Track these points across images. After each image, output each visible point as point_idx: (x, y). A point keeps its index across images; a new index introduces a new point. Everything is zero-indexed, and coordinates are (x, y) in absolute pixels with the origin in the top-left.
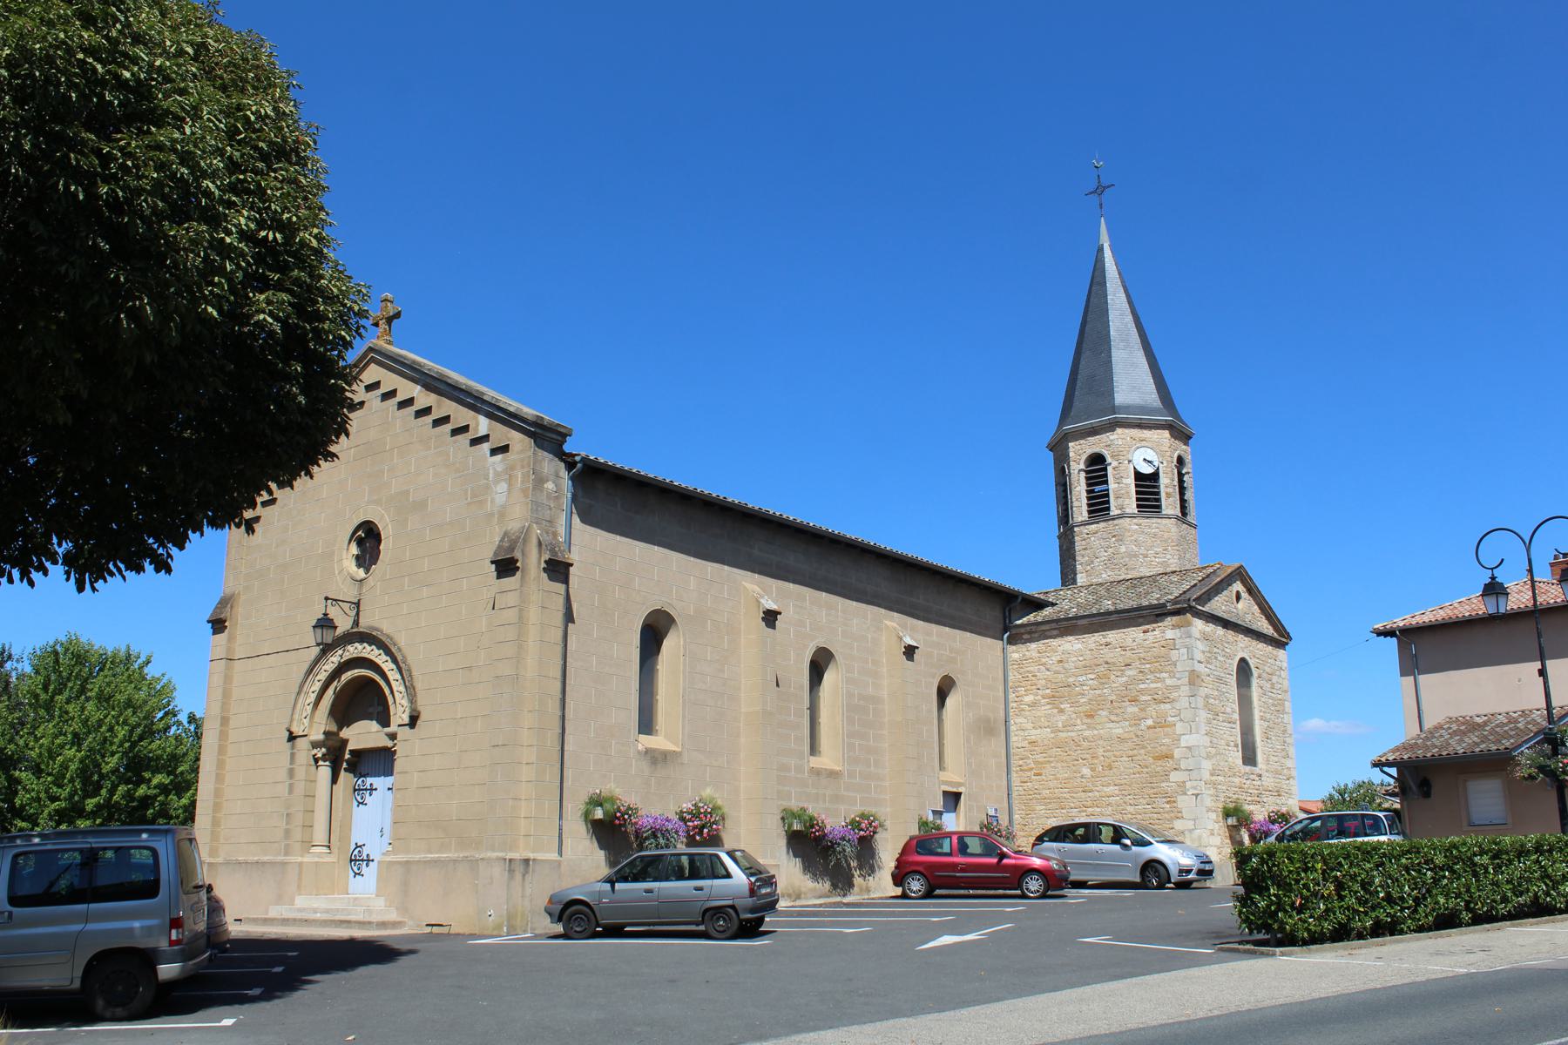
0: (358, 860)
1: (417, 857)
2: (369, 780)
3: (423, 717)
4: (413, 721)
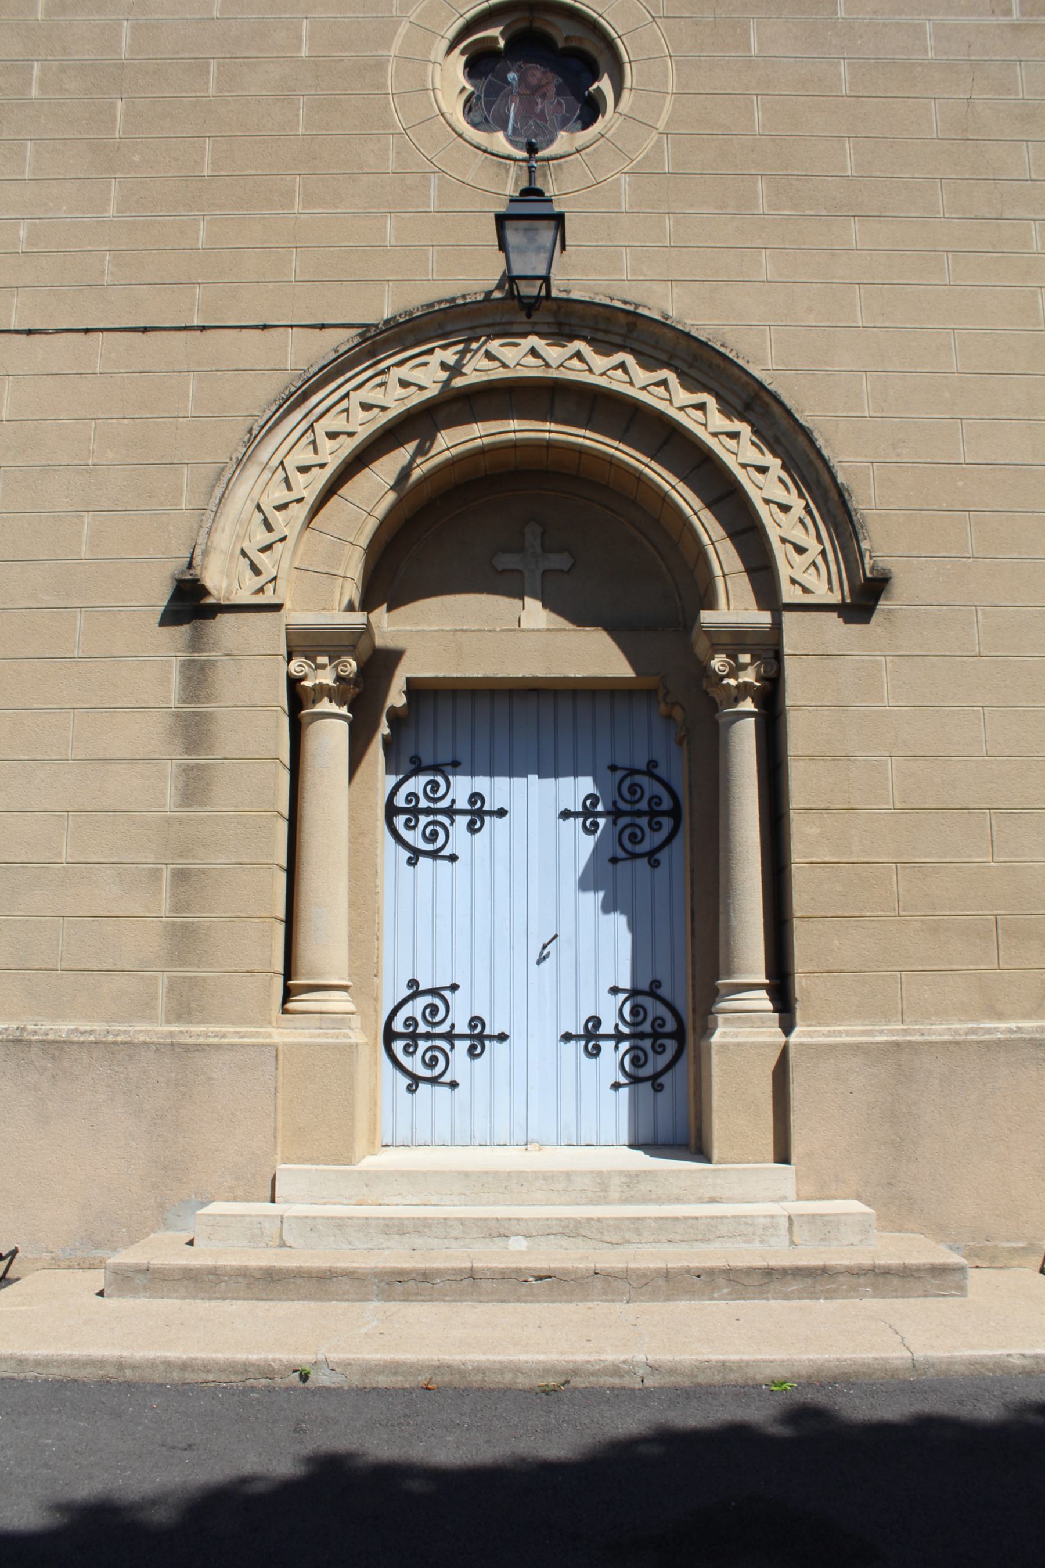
0: (424, 1037)
1: (940, 1030)
2: (460, 788)
3: (901, 589)
4: (864, 597)
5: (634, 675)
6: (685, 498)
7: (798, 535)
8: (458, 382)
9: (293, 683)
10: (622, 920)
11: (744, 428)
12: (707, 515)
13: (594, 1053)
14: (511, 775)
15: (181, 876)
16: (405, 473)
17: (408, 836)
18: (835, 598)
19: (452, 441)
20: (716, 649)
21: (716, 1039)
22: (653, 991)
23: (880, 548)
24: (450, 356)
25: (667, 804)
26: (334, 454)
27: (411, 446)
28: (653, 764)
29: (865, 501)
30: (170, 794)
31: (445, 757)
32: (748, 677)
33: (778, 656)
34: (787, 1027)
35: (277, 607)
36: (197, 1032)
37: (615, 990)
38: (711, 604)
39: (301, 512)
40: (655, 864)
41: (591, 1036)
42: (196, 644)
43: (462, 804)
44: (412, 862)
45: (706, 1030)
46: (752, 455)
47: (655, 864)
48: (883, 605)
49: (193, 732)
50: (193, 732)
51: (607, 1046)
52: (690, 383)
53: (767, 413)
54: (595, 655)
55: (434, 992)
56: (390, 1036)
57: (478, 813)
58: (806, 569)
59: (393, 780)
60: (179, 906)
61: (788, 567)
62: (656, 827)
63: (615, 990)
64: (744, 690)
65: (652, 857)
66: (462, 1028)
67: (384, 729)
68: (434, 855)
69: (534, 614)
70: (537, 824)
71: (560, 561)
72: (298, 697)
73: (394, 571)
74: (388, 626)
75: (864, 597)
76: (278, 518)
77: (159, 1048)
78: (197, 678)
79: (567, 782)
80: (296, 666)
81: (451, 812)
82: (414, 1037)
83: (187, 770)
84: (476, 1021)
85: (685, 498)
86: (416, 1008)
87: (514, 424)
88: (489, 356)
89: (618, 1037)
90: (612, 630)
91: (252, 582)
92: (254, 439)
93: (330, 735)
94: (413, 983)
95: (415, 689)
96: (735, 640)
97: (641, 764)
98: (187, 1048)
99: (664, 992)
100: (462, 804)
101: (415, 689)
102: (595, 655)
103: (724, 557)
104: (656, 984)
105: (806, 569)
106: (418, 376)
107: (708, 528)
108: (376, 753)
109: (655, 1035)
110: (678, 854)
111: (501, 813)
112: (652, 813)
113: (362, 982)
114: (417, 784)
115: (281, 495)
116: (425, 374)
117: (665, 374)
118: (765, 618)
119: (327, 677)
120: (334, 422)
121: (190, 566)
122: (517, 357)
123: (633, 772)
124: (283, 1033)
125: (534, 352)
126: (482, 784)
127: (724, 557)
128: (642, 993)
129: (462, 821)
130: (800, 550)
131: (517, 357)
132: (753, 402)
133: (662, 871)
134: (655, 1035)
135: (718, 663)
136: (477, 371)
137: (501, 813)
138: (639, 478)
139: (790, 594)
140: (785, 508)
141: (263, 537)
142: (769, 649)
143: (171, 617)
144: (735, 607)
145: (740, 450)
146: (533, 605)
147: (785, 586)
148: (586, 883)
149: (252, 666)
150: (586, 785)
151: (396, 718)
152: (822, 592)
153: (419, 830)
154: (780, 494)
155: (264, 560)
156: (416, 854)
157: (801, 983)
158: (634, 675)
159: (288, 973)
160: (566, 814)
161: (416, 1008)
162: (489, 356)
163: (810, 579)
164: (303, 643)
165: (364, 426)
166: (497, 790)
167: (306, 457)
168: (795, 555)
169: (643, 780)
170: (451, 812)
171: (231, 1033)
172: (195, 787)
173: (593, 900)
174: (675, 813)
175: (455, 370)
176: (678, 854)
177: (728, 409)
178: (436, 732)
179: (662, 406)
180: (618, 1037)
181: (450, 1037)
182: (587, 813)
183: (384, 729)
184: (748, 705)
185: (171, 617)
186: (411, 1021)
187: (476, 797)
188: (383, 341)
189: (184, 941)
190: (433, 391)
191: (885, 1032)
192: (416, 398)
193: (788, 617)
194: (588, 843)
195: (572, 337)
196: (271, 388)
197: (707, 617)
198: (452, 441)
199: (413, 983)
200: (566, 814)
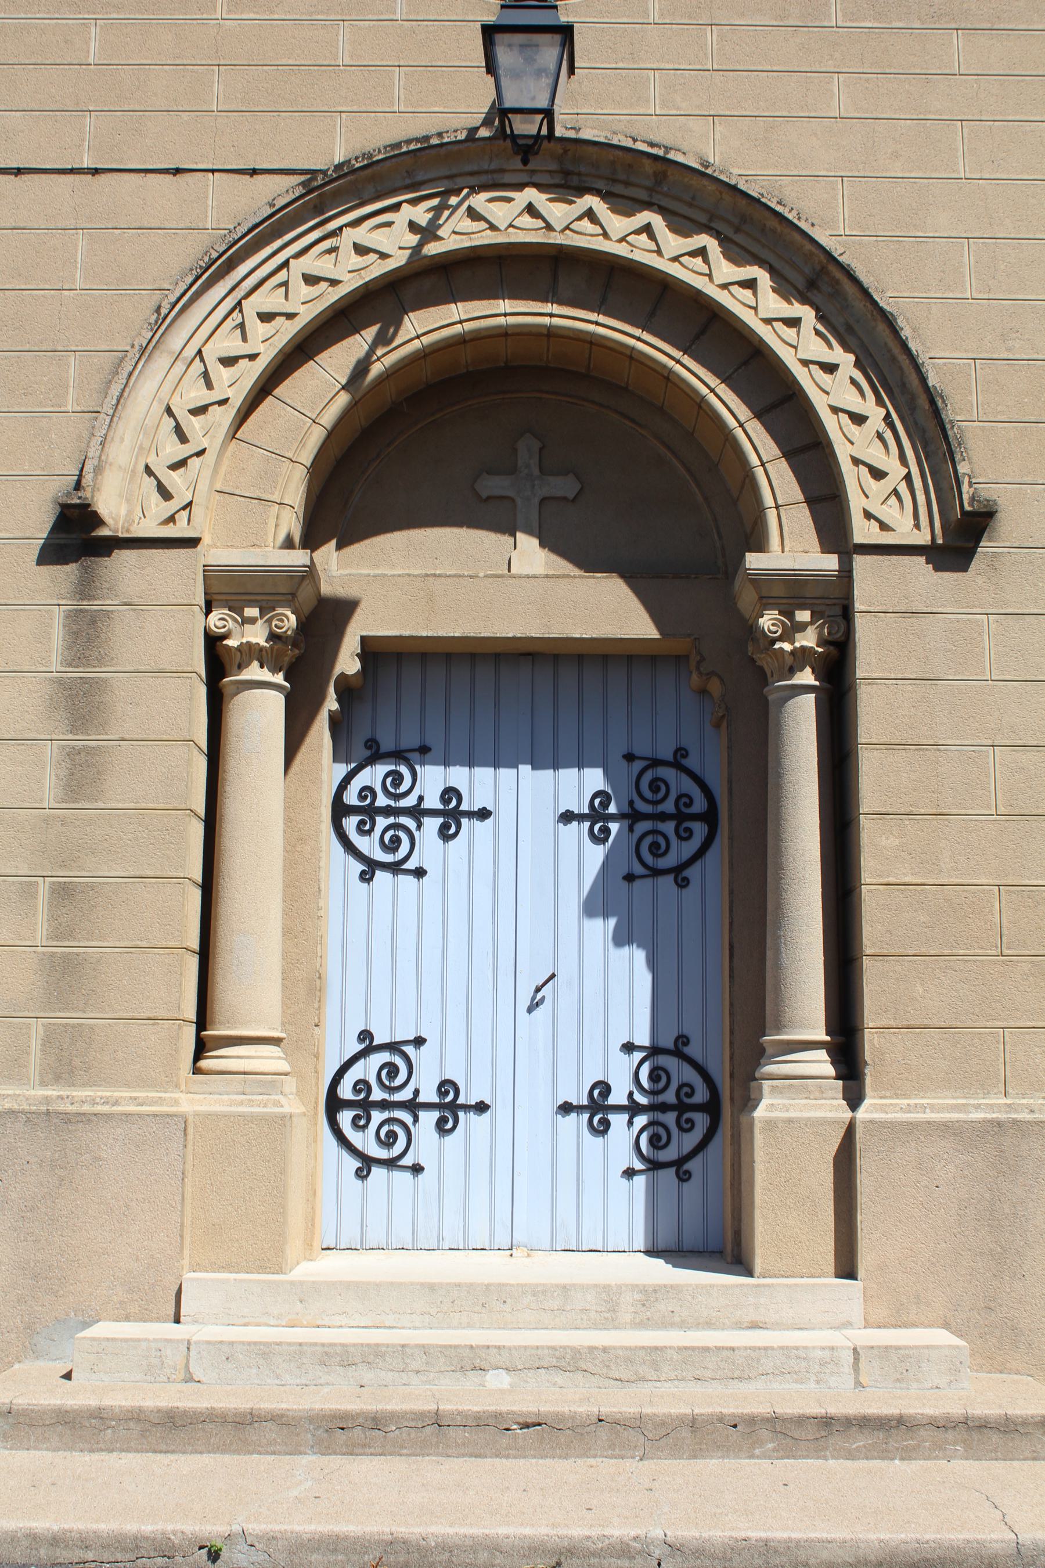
2: (431, 781)
5: (658, 637)
6: (729, 406)
7: (875, 455)
8: (432, 249)
9: (213, 642)
10: (640, 956)
11: (807, 314)
12: (756, 428)
13: (602, 1129)
14: (496, 765)
15: (63, 893)
16: (362, 368)
17: (362, 843)
18: (923, 538)
19: (425, 326)
20: (765, 603)
21: (760, 1113)
22: (679, 1049)
23: (986, 469)
24: (421, 214)
25: (699, 805)
26: (269, 342)
27: (370, 333)
28: (681, 752)
29: (962, 410)
30: (48, 787)
31: (410, 740)
32: (808, 639)
33: (846, 613)
34: (854, 1100)
35: (192, 542)
36: (80, 1097)
37: (629, 1048)
38: (760, 546)
39: (223, 417)
40: (683, 883)
41: (597, 1107)
42: (85, 589)
43: (433, 802)
44: (366, 877)
45: (748, 1101)
46: (816, 348)
47: (683, 883)
48: (985, 547)
49: (81, 703)
50: (81, 703)
51: (618, 1120)
52: (736, 253)
53: (837, 293)
54: (609, 610)
55: (393, 1047)
56: (334, 1104)
57: (452, 815)
58: (886, 501)
59: (342, 770)
60: (60, 932)
61: (861, 495)
62: (685, 836)
63: (629, 1048)
64: (802, 657)
65: (679, 874)
66: (428, 1095)
67: (331, 703)
68: (395, 868)
69: (529, 554)
70: (532, 827)
71: (564, 486)
72: (218, 660)
73: (347, 495)
74: (337, 569)
75: (961, 538)
76: (194, 425)
77: (30, 1118)
78: (86, 633)
79: (569, 775)
80: (216, 620)
81: (418, 812)
82: (365, 1106)
83: (72, 754)
84: (446, 1086)
85: (729, 406)
86: (369, 1068)
87: (504, 305)
88: (473, 214)
89: (633, 1109)
90: (622, 576)
91: (160, 508)
92: (163, 321)
93: (261, 710)
94: (365, 1035)
95: (372, 651)
96: (791, 591)
97: (666, 753)
98: (67, 1119)
99: (693, 1050)
100: (433, 802)
101: (372, 651)
102: (609, 610)
103: (778, 483)
104: (683, 1040)
105: (886, 501)
106: (379, 240)
107: (758, 444)
108: (320, 734)
109: (681, 1108)
110: (712, 873)
111: (483, 814)
112: (680, 817)
113: (295, 1038)
114: (374, 775)
115: (199, 395)
116: (387, 238)
117: (704, 240)
118: (831, 562)
119: (257, 635)
120: (267, 299)
121: (78, 486)
122: (508, 216)
123: (655, 763)
124: (195, 1099)
125: (531, 209)
126: (458, 776)
127: (778, 483)
128: (664, 1052)
129: (432, 824)
130: (878, 474)
131: (508, 216)
132: (819, 279)
133: (692, 892)
134: (681, 1108)
135: (768, 621)
136: (457, 234)
137: (483, 814)
138: (668, 377)
139: (863, 532)
140: (859, 419)
141: (175, 450)
142: (835, 603)
143: (53, 553)
144: (791, 547)
145: (800, 342)
146: (527, 542)
147: (857, 520)
148: (595, 905)
149: (159, 618)
150: (595, 779)
151: (347, 690)
152: (906, 530)
153: (376, 835)
154: (852, 401)
155: (175, 480)
156: (370, 868)
157: (873, 1042)
158: (658, 637)
159: (202, 1021)
160: (567, 817)
161: (369, 1068)
162: (473, 214)
163: (890, 512)
164: (225, 590)
165: (308, 304)
166: (478, 784)
167: (233, 345)
168: (872, 481)
169: (669, 774)
170: (418, 812)
171: (126, 1099)
172: (82, 776)
173: (600, 929)
174: (710, 817)
175: (428, 233)
176: (712, 873)
177: (785, 288)
178: (396, 710)
179: (699, 283)
180: (633, 1109)
181: (413, 1106)
182: (596, 815)
183: (331, 703)
184: (806, 677)
185: (53, 553)
186: (360, 1086)
187: (450, 793)
188: (331, 193)
189: (65, 976)
190: (399, 259)
191: (983, 1107)
192: (377, 269)
193: (860, 563)
194: (596, 854)
195: (582, 191)
196: (187, 252)
197: (754, 561)
198: (425, 326)
199: (365, 1035)
200: (567, 817)
